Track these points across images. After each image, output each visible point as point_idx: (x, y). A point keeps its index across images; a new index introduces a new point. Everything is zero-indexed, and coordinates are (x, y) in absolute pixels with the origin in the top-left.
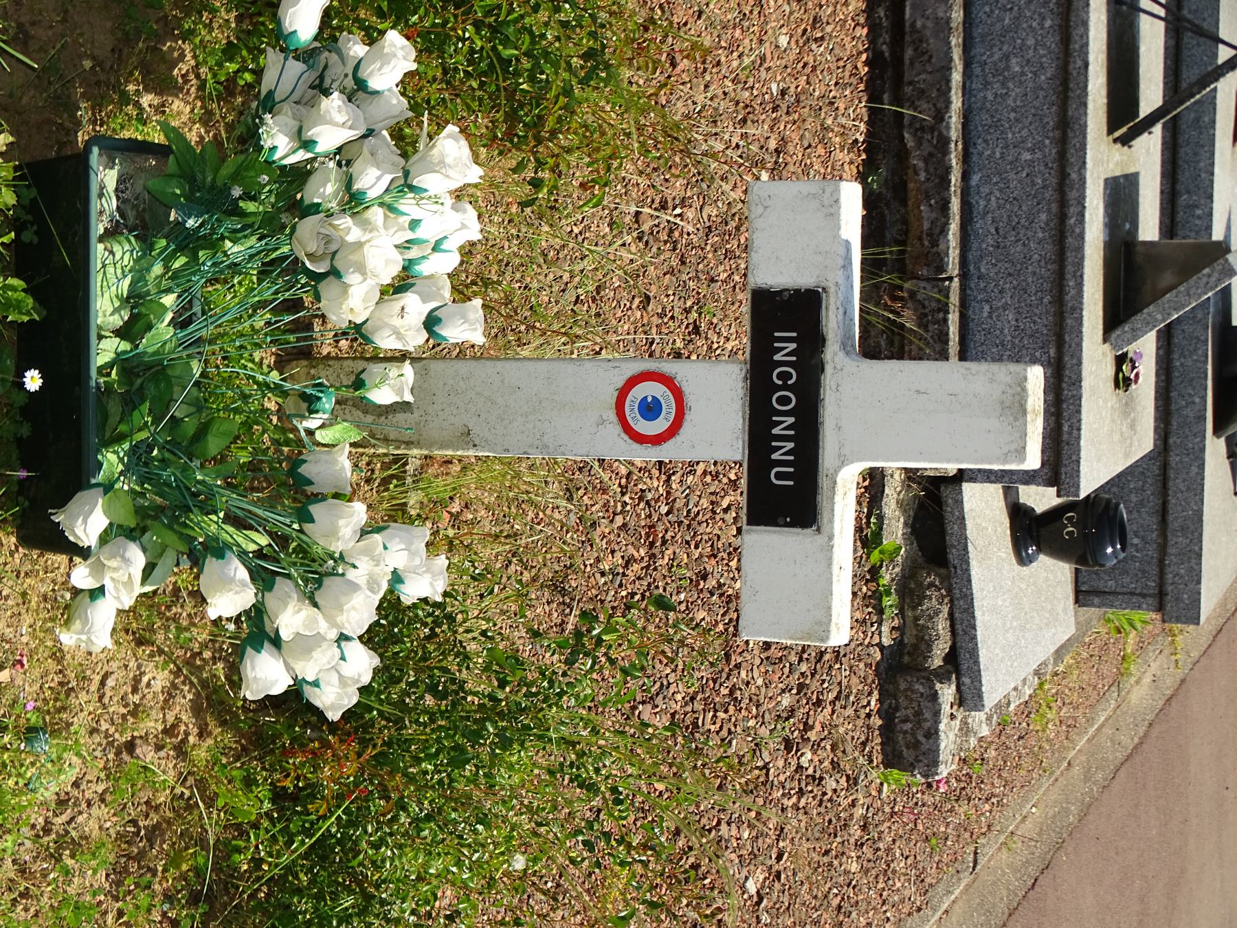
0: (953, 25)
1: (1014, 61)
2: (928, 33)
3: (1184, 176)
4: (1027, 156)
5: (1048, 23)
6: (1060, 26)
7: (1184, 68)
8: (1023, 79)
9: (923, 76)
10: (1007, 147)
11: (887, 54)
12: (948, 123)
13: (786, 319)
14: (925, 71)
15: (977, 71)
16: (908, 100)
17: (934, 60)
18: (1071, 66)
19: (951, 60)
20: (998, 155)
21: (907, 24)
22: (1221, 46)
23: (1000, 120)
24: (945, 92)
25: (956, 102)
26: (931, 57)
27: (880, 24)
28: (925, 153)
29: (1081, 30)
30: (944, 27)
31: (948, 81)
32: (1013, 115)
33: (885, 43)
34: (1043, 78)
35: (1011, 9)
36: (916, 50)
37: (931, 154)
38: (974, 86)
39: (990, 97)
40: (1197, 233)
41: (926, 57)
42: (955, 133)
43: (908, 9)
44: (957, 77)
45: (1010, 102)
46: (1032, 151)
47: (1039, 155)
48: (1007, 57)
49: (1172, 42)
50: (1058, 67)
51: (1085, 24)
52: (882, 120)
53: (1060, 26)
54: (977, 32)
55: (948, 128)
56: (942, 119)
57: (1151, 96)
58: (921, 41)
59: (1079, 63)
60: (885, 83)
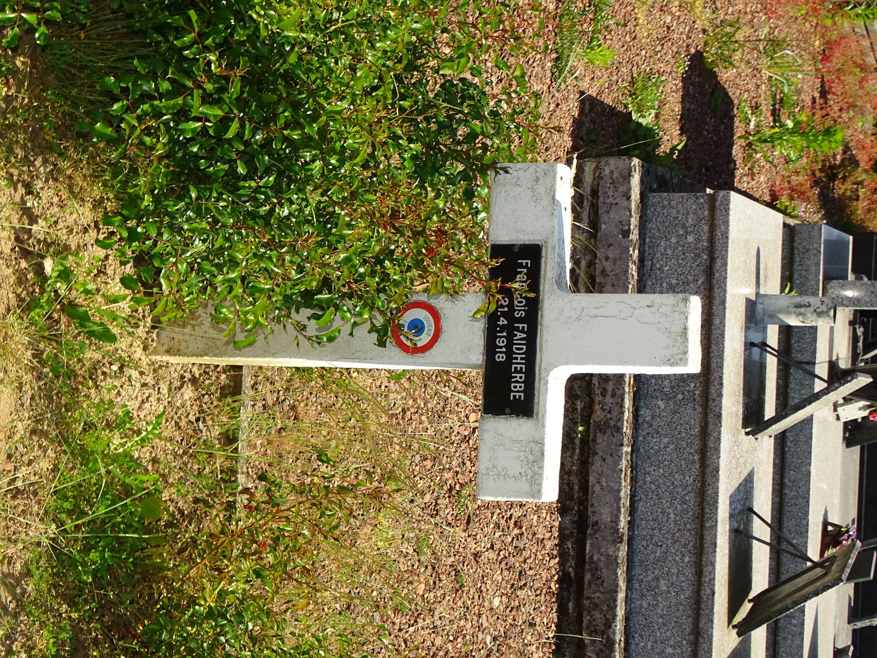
0: (620, 561)
1: (662, 582)
2: (602, 565)
3: (790, 475)
4: (670, 650)
5: (687, 559)
6: (695, 562)
7: (785, 519)
8: (669, 596)
9: (597, 595)
10: (656, 642)
11: (572, 575)
12: (614, 630)
13: (517, 263)
14: (599, 591)
15: (637, 585)
16: (587, 610)
17: (605, 584)
18: (703, 592)
19: (617, 585)
20: (649, 647)
21: (587, 557)
22: (816, 380)
23: (651, 622)
24: (613, 608)
25: (620, 612)
26: (603, 582)
27: (569, 552)
28: (597, 649)
29: (710, 568)
30: (613, 562)
31: (615, 600)
32: (660, 620)
33: (571, 566)
34: (682, 597)
35: (661, 546)
36: (593, 575)
37: (601, 650)
38: (634, 596)
39: (645, 605)
40: (793, 636)
41: (600, 581)
42: (619, 636)
43: (588, 546)
44: (621, 596)
45: (659, 610)
46: (674, 647)
47: (678, 651)
48: (657, 579)
49: (777, 500)
50: (693, 591)
51: (713, 564)
52: (567, 621)
53: (695, 562)
54: (636, 559)
55: (614, 633)
56: (610, 627)
57: (760, 581)
58: (597, 570)
59: (708, 591)
60: (570, 594)
